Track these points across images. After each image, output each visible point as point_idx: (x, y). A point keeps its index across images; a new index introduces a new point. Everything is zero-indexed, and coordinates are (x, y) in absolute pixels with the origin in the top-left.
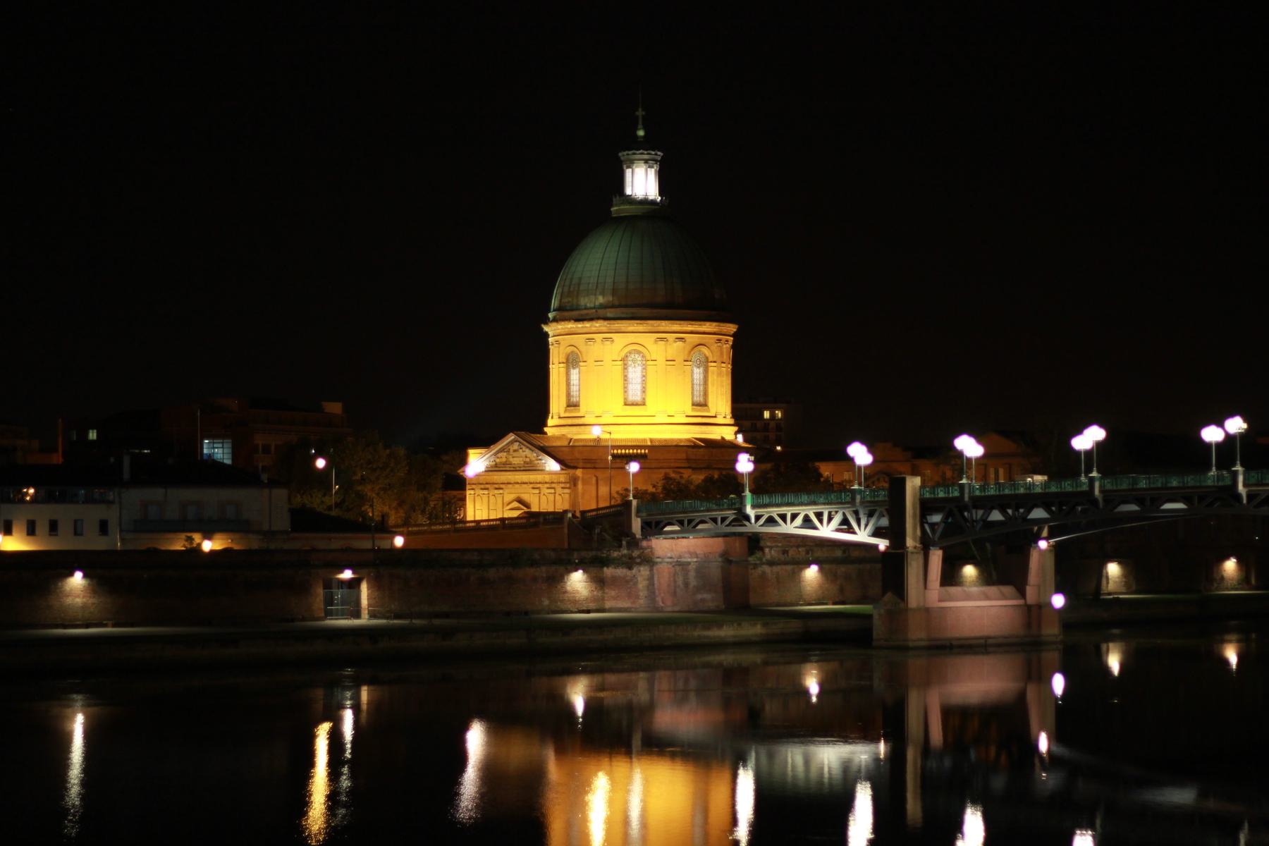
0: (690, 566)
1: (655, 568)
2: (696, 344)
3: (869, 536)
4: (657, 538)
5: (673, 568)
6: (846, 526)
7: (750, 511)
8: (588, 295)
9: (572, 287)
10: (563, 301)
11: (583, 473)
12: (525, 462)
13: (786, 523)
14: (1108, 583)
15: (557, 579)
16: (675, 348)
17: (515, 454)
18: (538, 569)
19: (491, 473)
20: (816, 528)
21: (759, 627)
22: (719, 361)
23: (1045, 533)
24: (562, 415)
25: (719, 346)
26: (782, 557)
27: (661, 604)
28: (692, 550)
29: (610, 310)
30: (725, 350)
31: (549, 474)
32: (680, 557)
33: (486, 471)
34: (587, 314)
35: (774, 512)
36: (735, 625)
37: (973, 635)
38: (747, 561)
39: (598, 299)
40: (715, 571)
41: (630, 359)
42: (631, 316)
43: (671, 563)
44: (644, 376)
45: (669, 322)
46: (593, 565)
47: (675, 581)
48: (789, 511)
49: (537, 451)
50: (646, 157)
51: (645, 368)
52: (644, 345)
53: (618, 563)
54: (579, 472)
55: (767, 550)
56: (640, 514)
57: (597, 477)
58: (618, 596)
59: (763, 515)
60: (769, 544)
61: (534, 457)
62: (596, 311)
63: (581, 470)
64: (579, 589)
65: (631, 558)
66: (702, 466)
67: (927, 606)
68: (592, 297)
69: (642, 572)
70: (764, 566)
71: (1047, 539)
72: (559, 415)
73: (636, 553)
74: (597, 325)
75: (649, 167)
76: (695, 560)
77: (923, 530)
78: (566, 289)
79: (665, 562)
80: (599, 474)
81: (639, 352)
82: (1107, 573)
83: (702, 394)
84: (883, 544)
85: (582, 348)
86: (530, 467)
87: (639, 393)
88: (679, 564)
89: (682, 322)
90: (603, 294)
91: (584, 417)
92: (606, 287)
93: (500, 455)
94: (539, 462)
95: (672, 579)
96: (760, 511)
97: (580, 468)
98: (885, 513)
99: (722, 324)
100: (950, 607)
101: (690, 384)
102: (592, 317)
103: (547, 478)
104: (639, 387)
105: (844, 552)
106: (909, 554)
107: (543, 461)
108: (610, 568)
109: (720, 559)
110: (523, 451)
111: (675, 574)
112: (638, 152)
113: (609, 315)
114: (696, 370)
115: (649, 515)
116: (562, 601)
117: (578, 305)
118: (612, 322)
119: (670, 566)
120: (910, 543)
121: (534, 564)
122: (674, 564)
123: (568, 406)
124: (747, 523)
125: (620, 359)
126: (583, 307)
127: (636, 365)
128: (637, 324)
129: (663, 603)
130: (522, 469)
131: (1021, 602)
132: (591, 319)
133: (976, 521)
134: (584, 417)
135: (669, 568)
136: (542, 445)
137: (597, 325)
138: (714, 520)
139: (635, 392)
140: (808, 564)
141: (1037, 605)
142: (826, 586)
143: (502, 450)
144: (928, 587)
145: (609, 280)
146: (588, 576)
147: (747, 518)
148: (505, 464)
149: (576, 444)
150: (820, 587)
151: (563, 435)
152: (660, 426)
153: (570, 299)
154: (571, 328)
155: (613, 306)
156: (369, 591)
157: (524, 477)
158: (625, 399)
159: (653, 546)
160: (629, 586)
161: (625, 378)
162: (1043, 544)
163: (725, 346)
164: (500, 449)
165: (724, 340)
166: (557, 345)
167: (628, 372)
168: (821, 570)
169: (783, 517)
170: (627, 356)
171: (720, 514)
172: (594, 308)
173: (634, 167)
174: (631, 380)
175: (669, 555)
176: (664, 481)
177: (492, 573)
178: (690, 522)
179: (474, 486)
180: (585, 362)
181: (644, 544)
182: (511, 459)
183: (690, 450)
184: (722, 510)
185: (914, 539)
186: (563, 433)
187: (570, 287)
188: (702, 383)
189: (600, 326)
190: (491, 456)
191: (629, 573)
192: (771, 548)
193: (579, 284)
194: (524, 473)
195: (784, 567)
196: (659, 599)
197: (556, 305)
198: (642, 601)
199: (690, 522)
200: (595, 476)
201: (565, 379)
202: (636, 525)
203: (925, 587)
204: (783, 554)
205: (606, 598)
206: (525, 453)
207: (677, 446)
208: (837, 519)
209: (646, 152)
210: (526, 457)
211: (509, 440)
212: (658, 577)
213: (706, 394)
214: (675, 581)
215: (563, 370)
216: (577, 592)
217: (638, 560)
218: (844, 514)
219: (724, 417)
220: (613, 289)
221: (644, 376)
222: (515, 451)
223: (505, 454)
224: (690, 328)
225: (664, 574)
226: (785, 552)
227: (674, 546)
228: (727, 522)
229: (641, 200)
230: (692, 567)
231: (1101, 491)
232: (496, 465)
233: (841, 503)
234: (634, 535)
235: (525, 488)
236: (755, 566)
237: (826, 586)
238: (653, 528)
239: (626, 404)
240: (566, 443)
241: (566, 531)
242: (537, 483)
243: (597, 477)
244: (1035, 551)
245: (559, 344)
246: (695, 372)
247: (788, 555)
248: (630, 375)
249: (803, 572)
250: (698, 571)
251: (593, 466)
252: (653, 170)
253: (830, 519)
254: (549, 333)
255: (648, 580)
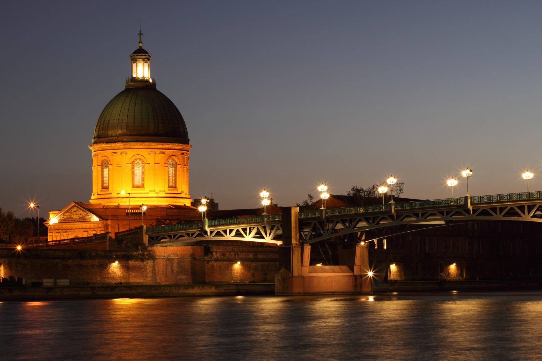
0: (174, 261)
1: (156, 262)
2: (170, 155)
3: (271, 240)
4: (157, 246)
5: (165, 262)
6: (259, 235)
7: (207, 229)
8: (113, 130)
9: (105, 125)
10: (99, 132)
11: (111, 223)
12: (80, 217)
13: (226, 234)
14: (390, 275)
15: (104, 266)
16: (160, 157)
17: (75, 213)
18: (94, 261)
19: (61, 224)
20: (243, 237)
21: (213, 288)
22: (182, 165)
23: (363, 238)
24: (99, 193)
25: (183, 157)
26: (222, 258)
27: (159, 280)
28: (175, 252)
29: (125, 137)
30: (185, 159)
31: (93, 223)
32: (169, 256)
33: (59, 223)
34: (113, 139)
35: (220, 229)
36: (201, 287)
37: (327, 291)
38: (204, 259)
39: (118, 131)
40: (187, 264)
41: (136, 163)
42: (136, 140)
43: (164, 259)
44: (143, 172)
45: (157, 143)
46: (124, 259)
47: (166, 269)
48: (228, 228)
49: (86, 211)
50: (143, 57)
51: (143, 168)
52: (144, 156)
53: (136, 258)
54: (109, 222)
55: (214, 253)
56: (147, 233)
57: (119, 225)
58: (136, 276)
59: (214, 231)
60: (215, 250)
61: (85, 214)
62: (118, 138)
63: (110, 221)
64: (116, 272)
65: (143, 255)
66: (175, 219)
67: (303, 275)
68: (116, 130)
69: (149, 264)
70: (213, 262)
71: (364, 241)
72: (98, 193)
73: (146, 253)
74: (118, 145)
75: (145, 63)
76: (177, 258)
77: (300, 235)
78: (101, 126)
79: (161, 258)
80: (120, 223)
81: (140, 159)
82: (390, 270)
83: (174, 181)
84: (279, 243)
85: (110, 157)
86: (83, 220)
87: (140, 181)
88: (169, 259)
89: (163, 143)
90: (121, 129)
91: (111, 194)
92: (123, 125)
93: (67, 214)
94: (87, 217)
95: (165, 267)
96: (213, 229)
97: (110, 220)
98: (280, 227)
99: (184, 145)
100: (315, 276)
101: (168, 176)
102: (115, 140)
103: (92, 226)
104: (140, 178)
105: (254, 256)
106: (293, 248)
107: (90, 217)
108: (132, 261)
109: (190, 258)
110: (79, 212)
111: (166, 265)
112: (139, 55)
113: (124, 140)
114: (171, 169)
115: (152, 234)
116: (107, 278)
117: (108, 135)
118: (126, 143)
119: (164, 261)
120: (294, 242)
121: (92, 258)
122: (166, 259)
123: (102, 188)
124: (206, 236)
125: (130, 163)
126: (111, 136)
127: (139, 166)
128: (139, 144)
129: (160, 280)
130: (78, 221)
131: (352, 274)
132: (115, 142)
133: (329, 229)
134: (111, 194)
135: (163, 262)
136: (89, 208)
137: (118, 145)
138: (188, 235)
139: (138, 180)
140: (235, 261)
141: (359, 276)
142: (245, 273)
143: (67, 212)
144: (303, 265)
145: (125, 121)
146: (121, 265)
147: (206, 233)
148: (69, 219)
149: (107, 207)
150: (242, 273)
151: (100, 204)
152: (152, 198)
153: (104, 132)
154: (104, 147)
155: (126, 135)
156: (5, 271)
157: (79, 225)
158: (133, 184)
159: (155, 250)
160: (143, 271)
161: (133, 173)
162: (362, 243)
163: (185, 156)
164: (66, 211)
165: (185, 153)
166: (96, 156)
167: (134, 170)
168: (242, 264)
169: (225, 231)
170: (134, 161)
171: (191, 231)
172: (116, 136)
173: (137, 62)
174: (136, 174)
175: (163, 255)
176: (157, 223)
177: (70, 262)
178: (175, 236)
179: (52, 231)
180: (112, 164)
181: (150, 249)
182: (72, 216)
183: (168, 210)
184: (192, 229)
185: (296, 240)
186: (100, 203)
187: (103, 126)
188: (173, 176)
189: (119, 146)
190: (62, 214)
191: (142, 264)
192: (216, 252)
193: (108, 124)
194: (79, 223)
195: (223, 263)
196: (158, 278)
197: (96, 135)
198: (149, 279)
199: (175, 236)
200: (118, 224)
201: (101, 174)
202: (146, 239)
203: (302, 266)
204: (223, 256)
205: (130, 277)
206: (80, 213)
207: (161, 208)
208: (254, 232)
209: (143, 55)
210: (80, 215)
211: (71, 206)
212: (158, 266)
213: (176, 182)
214: (166, 269)
215: (100, 169)
216: (115, 273)
217: (147, 257)
218: (258, 229)
219: (185, 194)
220: (127, 126)
221: (143, 172)
222: (75, 211)
223: (69, 213)
224: (167, 147)
225: (161, 264)
226: (224, 255)
227: (166, 250)
228: (195, 235)
229: (141, 80)
230: (175, 261)
231: (395, 211)
232: (64, 220)
233: (257, 223)
234: (145, 244)
235: (80, 231)
236: (208, 262)
237: (245, 273)
238: (155, 240)
239: (133, 187)
240: (102, 207)
241: (108, 243)
242: (87, 228)
243: (119, 225)
244: (358, 247)
245: (98, 155)
246: (170, 170)
247: (225, 257)
248: (136, 171)
249: (233, 266)
250: (178, 263)
251: (116, 219)
252: (147, 64)
253: (250, 232)
254: (92, 150)
255: (152, 267)
